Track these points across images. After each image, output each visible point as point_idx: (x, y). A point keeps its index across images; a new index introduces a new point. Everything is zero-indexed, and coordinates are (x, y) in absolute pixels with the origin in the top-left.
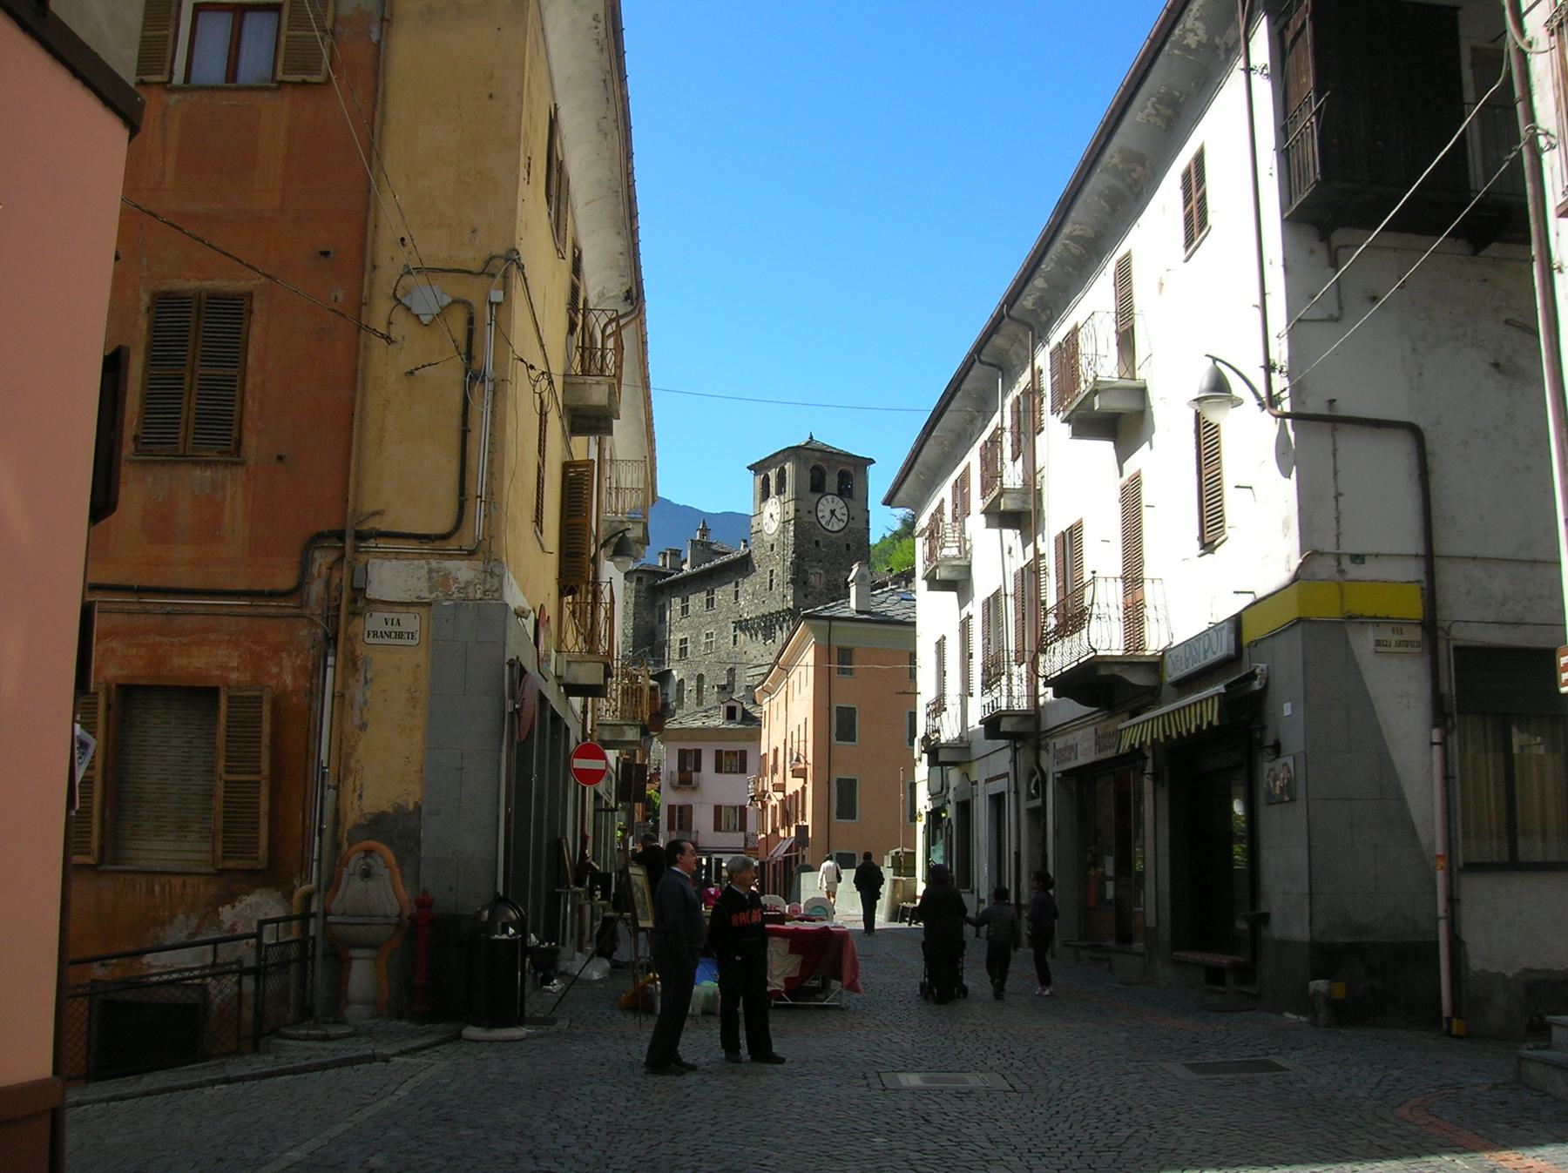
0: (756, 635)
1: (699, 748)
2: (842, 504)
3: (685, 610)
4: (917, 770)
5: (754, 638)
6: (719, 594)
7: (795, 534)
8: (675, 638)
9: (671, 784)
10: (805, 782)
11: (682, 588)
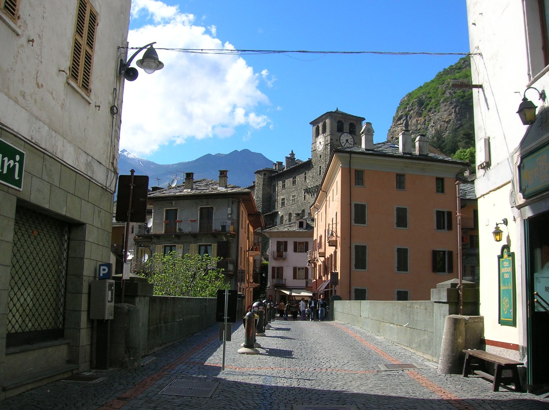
0: (314, 195)
1: (286, 240)
2: (351, 137)
3: (284, 186)
5: (313, 196)
6: (298, 179)
7: (330, 150)
8: (280, 198)
10: (336, 248)
11: (283, 177)
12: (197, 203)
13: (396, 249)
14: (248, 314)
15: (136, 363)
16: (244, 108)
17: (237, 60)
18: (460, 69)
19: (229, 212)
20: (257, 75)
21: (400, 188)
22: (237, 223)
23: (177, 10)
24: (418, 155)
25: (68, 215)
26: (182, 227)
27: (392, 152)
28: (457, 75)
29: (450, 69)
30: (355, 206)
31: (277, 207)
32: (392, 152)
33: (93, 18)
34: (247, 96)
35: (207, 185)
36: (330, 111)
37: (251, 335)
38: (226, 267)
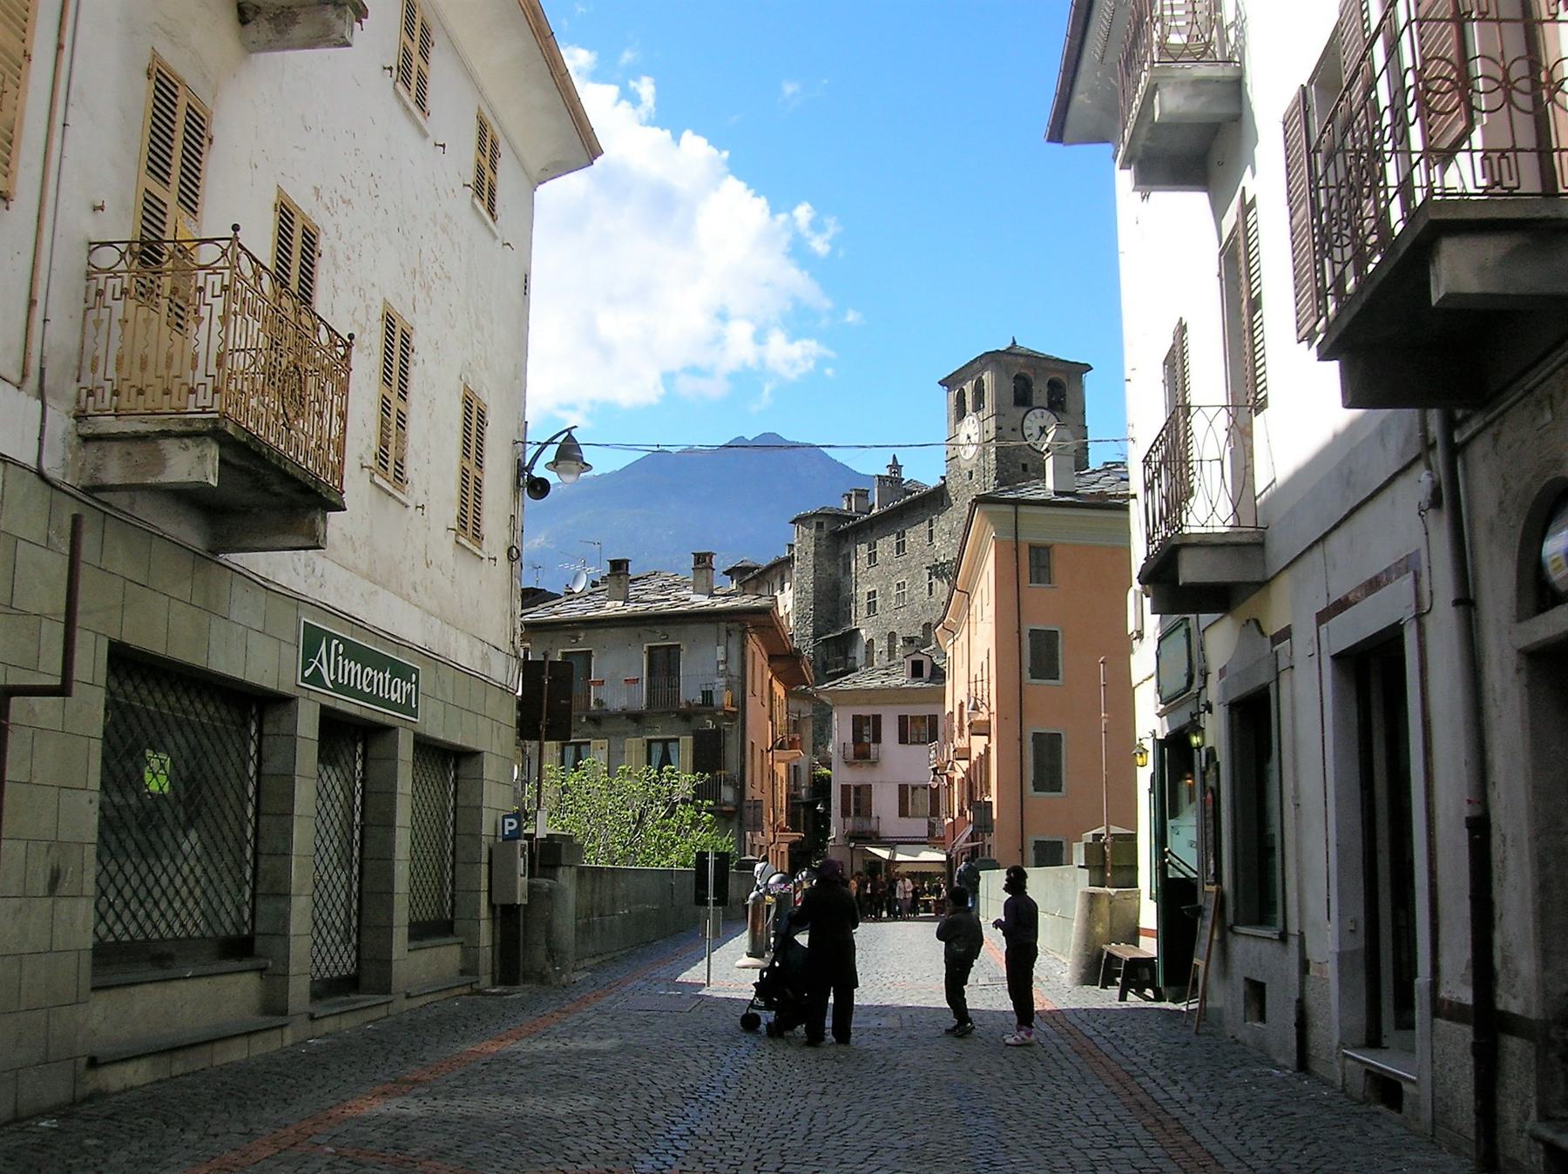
3: (872, 557)
4: (1135, 660)
8: (862, 592)
12: (639, 636)
14: (752, 895)
22: (740, 684)
25: (464, 744)
31: (856, 616)
33: (481, 415)
36: (993, 349)
38: (716, 796)
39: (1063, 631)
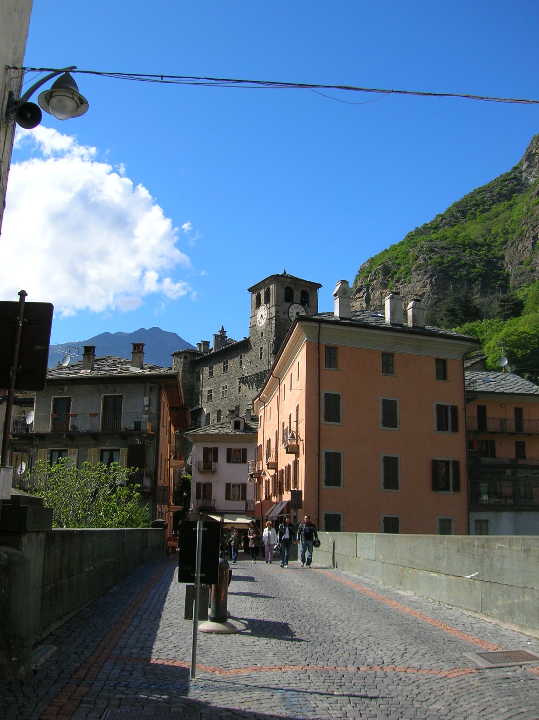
0: (252, 386)
2: (303, 309)
3: (211, 373)
5: (251, 387)
6: (231, 364)
8: (205, 390)
9: (199, 469)
13: (382, 459)
15: (22, 668)
16: (157, 271)
17: (151, 208)
18: (436, 228)
19: (146, 403)
20: (176, 229)
21: (387, 373)
23: (74, 141)
24: (412, 327)
26: (76, 424)
27: (376, 322)
28: (433, 236)
29: (423, 228)
30: (325, 397)
31: (202, 401)
32: (376, 322)
34: (162, 256)
35: (113, 365)
36: (276, 274)
37: (223, 599)
39: (342, 394)
